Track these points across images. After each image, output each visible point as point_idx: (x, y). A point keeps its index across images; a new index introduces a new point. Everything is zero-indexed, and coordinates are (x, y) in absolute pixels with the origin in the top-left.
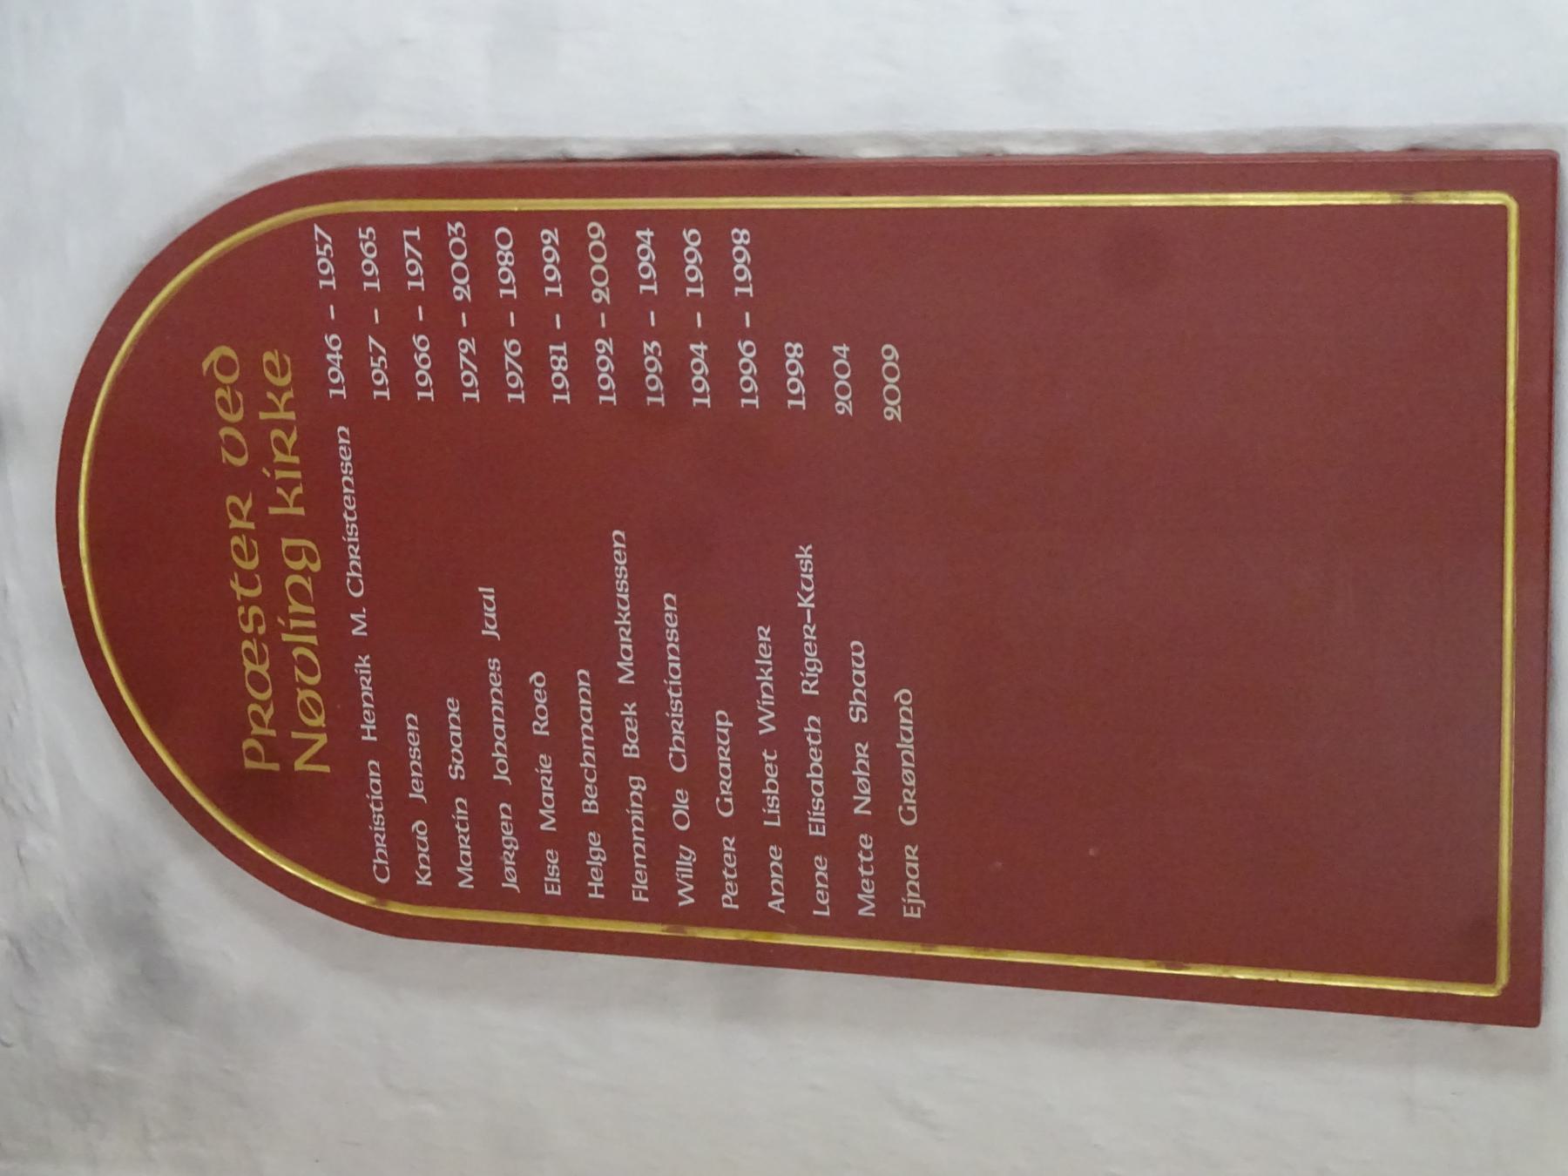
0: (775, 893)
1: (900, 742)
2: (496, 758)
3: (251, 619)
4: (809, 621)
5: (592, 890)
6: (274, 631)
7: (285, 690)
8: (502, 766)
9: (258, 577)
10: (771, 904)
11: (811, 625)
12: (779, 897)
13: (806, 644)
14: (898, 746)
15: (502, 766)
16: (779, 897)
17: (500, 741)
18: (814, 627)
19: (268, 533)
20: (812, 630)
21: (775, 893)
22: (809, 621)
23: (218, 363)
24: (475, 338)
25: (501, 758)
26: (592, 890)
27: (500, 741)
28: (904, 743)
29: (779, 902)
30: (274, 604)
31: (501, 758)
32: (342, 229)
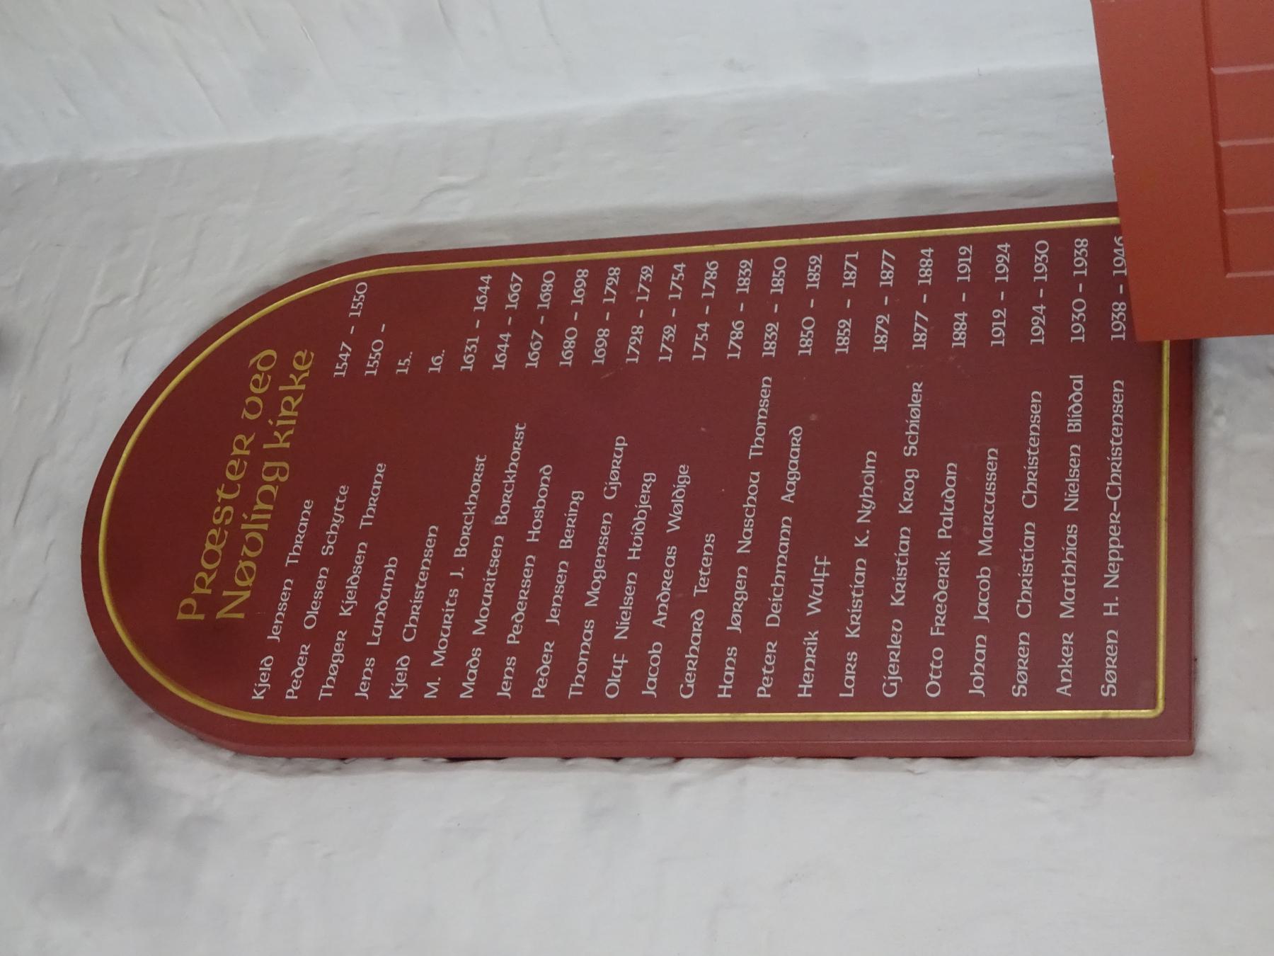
0: (1064, 680)
1: (943, 511)
2: (974, 676)
3: (222, 515)
4: (1115, 509)
5: (801, 691)
6: (238, 520)
7: (231, 555)
8: (978, 683)
9: (239, 485)
10: (1058, 690)
11: (1117, 513)
12: (1067, 684)
13: (1111, 527)
14: (941, 514)
15: (978, 683)
16: (1067, 684)
17: (980, 663)
18: (1119, 515)
19: (258, 456)
20: (1117, 517)
21: (1064, 680)
22: (1115, 509)
23: (262, 360)
24: (573, 319)
25: (978, 675)
26: (801, 691)
27: (980, 663)
28: (946, 511)
29: (1066, 687)
30: (244, 505)
31: (978, 675)
32: (501, 276)
